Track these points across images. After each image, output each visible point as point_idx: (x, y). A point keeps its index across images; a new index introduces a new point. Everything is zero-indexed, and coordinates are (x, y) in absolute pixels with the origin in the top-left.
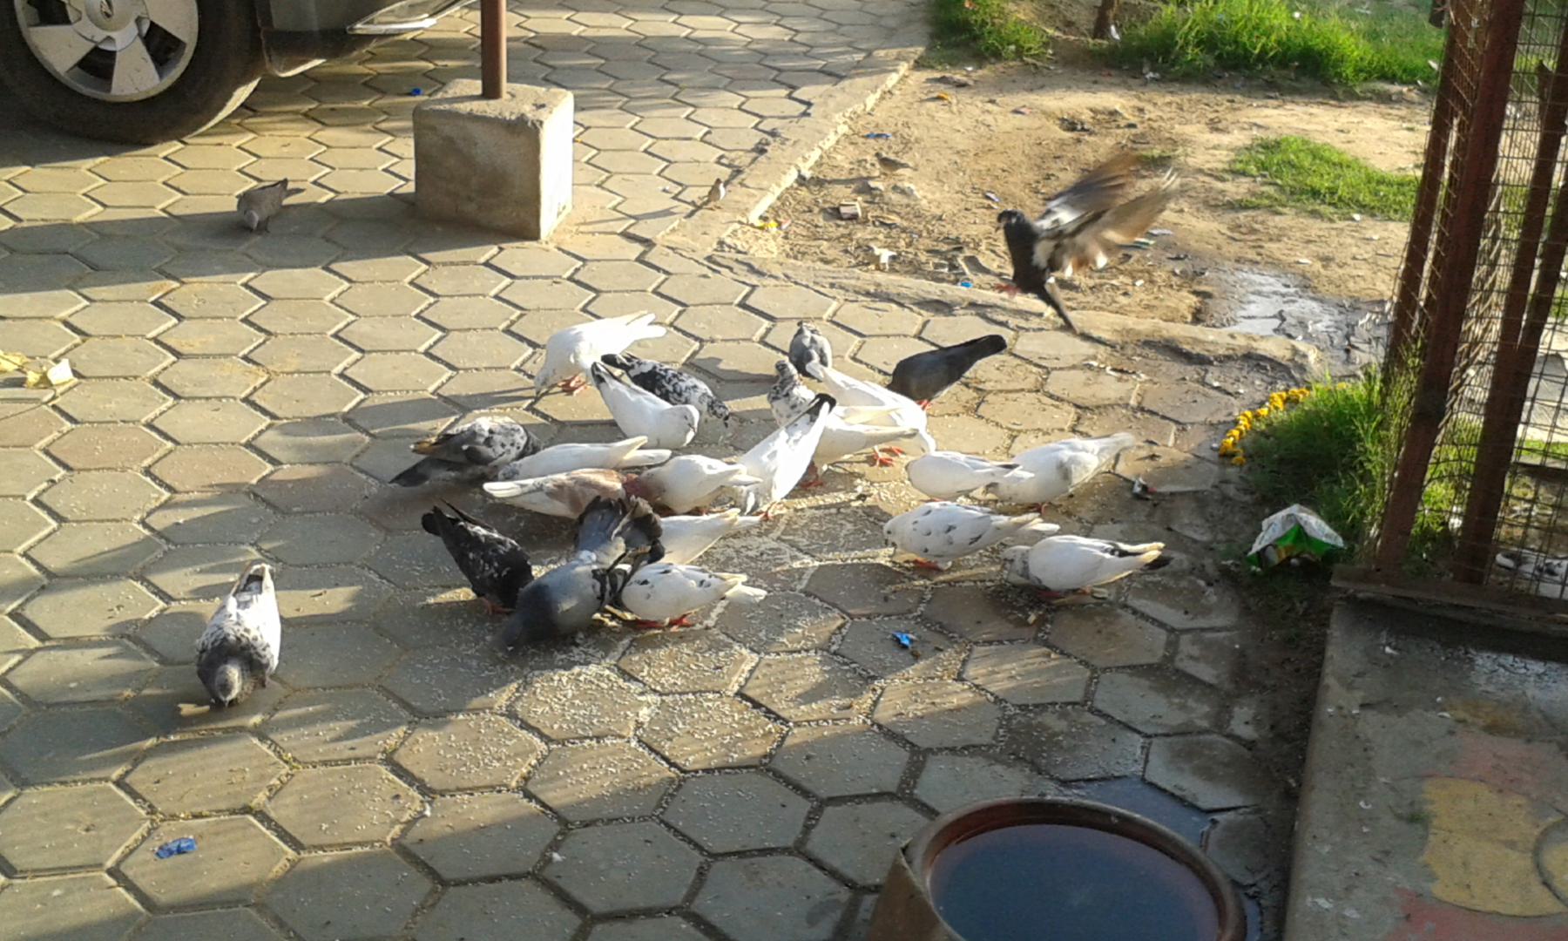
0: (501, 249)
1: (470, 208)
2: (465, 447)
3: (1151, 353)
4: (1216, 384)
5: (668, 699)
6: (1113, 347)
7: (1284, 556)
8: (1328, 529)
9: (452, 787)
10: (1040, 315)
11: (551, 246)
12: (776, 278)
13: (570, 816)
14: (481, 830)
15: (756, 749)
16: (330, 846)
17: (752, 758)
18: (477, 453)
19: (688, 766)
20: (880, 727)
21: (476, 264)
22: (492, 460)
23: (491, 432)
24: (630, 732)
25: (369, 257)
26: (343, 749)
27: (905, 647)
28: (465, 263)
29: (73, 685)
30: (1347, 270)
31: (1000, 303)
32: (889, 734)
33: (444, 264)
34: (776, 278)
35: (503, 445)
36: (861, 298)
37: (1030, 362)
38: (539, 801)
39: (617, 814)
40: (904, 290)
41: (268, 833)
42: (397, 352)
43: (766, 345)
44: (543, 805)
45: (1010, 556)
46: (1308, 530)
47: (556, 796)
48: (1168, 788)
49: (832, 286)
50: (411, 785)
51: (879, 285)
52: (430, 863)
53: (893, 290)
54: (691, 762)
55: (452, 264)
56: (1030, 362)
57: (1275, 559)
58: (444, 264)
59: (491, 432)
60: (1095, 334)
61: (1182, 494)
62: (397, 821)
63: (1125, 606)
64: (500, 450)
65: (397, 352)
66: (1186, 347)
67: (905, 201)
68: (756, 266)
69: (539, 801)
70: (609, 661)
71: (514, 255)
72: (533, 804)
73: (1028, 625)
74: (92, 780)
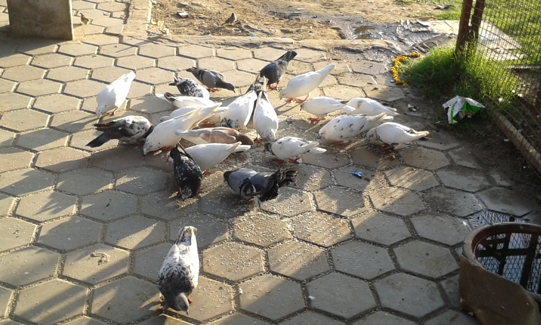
0: (59, 46)
1: (37, 30)
2: (120, 129)
3: (340, 52)
4: (371, 59)
5: (294, 218)
6: (326, 51)
7: (464, 115)
8: (477, 103)
9: (241, 278)
10: (292, 43)
11: (79, 42)
12: (182, 43)
13: (301, 278)
14: (269, 294)
15: (345, 231)
16: (211, 318)
17: (347, 235)
18: (126, 131)
19: (327, 245)
20: (381, 211)
21: (53, 53)
22: (133, 135)
23: (133, 122)
24: (290, 236)
25: (2, 57)
26: (52, 217)
27: (360, 177)
28: (48, 53)
29: (26, 273)
30: (374, 15)
31: (274, 41)
32: (387, 213)
33: (39, 55)
34: (182, 43)
35: (138, 129)
36: (221, 46)
37: (302, 61)
38: (282, 275)
39: (319, 273)
40: (236, 41)
41: (178, 319)
42: (50, 94)
43: (18, 92)
44: (284, 276)
45: (371, 134)
46: (471, 104)
47: (287, 270)
48: (500, 211)
49: (207, 43)
50: (222, 281)
51: (224, 40)
52: (261, 314)
53: (232, 42)
54: (326, 242)
55: (42, 54)
56: (302, 61)
57: (462, 116)
58: (39, 55)
59: (133, 122)
60: (317, 47)
61: (398, 100)
62: (230, 300)
63: (419, 146)
64: (137, 130)
65: (50, 94)
66: (351, 48)
67: (201, 8)
68: (171, 39)
69: (282, 275)
70: (255, 209)
71: (65, 46)
72: (280, 277)
73: (394, 159)
74: (75, 317)
